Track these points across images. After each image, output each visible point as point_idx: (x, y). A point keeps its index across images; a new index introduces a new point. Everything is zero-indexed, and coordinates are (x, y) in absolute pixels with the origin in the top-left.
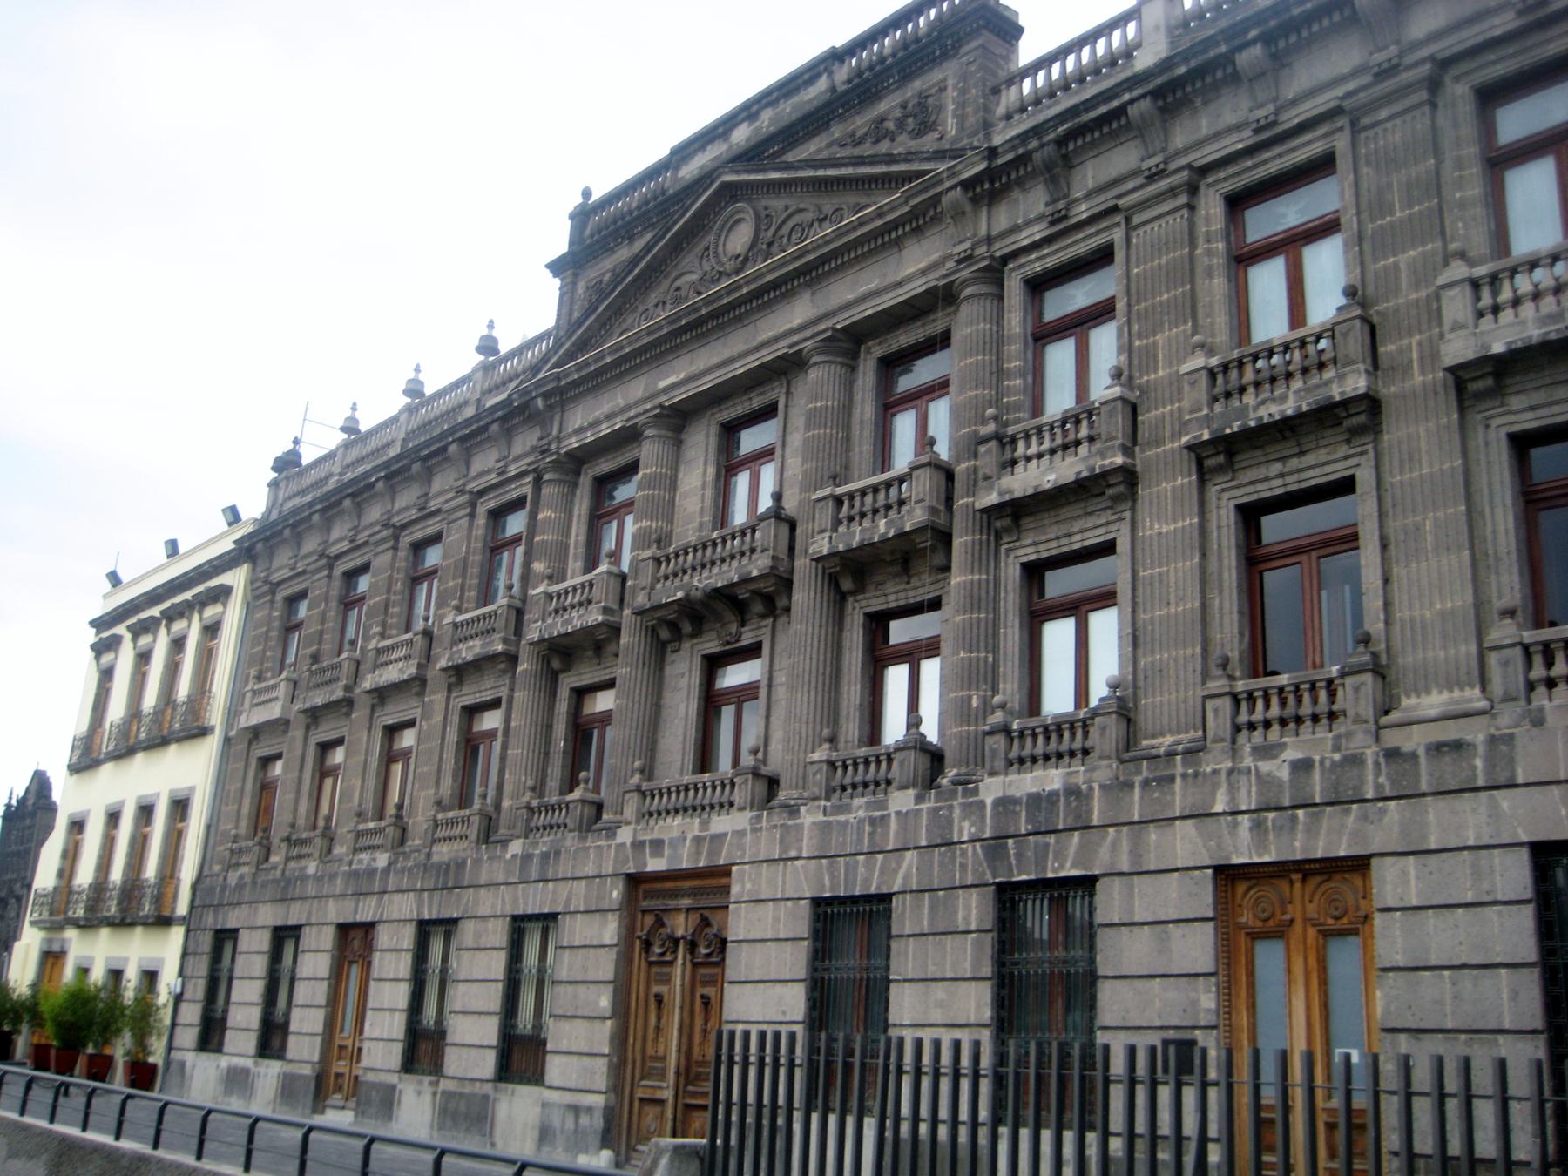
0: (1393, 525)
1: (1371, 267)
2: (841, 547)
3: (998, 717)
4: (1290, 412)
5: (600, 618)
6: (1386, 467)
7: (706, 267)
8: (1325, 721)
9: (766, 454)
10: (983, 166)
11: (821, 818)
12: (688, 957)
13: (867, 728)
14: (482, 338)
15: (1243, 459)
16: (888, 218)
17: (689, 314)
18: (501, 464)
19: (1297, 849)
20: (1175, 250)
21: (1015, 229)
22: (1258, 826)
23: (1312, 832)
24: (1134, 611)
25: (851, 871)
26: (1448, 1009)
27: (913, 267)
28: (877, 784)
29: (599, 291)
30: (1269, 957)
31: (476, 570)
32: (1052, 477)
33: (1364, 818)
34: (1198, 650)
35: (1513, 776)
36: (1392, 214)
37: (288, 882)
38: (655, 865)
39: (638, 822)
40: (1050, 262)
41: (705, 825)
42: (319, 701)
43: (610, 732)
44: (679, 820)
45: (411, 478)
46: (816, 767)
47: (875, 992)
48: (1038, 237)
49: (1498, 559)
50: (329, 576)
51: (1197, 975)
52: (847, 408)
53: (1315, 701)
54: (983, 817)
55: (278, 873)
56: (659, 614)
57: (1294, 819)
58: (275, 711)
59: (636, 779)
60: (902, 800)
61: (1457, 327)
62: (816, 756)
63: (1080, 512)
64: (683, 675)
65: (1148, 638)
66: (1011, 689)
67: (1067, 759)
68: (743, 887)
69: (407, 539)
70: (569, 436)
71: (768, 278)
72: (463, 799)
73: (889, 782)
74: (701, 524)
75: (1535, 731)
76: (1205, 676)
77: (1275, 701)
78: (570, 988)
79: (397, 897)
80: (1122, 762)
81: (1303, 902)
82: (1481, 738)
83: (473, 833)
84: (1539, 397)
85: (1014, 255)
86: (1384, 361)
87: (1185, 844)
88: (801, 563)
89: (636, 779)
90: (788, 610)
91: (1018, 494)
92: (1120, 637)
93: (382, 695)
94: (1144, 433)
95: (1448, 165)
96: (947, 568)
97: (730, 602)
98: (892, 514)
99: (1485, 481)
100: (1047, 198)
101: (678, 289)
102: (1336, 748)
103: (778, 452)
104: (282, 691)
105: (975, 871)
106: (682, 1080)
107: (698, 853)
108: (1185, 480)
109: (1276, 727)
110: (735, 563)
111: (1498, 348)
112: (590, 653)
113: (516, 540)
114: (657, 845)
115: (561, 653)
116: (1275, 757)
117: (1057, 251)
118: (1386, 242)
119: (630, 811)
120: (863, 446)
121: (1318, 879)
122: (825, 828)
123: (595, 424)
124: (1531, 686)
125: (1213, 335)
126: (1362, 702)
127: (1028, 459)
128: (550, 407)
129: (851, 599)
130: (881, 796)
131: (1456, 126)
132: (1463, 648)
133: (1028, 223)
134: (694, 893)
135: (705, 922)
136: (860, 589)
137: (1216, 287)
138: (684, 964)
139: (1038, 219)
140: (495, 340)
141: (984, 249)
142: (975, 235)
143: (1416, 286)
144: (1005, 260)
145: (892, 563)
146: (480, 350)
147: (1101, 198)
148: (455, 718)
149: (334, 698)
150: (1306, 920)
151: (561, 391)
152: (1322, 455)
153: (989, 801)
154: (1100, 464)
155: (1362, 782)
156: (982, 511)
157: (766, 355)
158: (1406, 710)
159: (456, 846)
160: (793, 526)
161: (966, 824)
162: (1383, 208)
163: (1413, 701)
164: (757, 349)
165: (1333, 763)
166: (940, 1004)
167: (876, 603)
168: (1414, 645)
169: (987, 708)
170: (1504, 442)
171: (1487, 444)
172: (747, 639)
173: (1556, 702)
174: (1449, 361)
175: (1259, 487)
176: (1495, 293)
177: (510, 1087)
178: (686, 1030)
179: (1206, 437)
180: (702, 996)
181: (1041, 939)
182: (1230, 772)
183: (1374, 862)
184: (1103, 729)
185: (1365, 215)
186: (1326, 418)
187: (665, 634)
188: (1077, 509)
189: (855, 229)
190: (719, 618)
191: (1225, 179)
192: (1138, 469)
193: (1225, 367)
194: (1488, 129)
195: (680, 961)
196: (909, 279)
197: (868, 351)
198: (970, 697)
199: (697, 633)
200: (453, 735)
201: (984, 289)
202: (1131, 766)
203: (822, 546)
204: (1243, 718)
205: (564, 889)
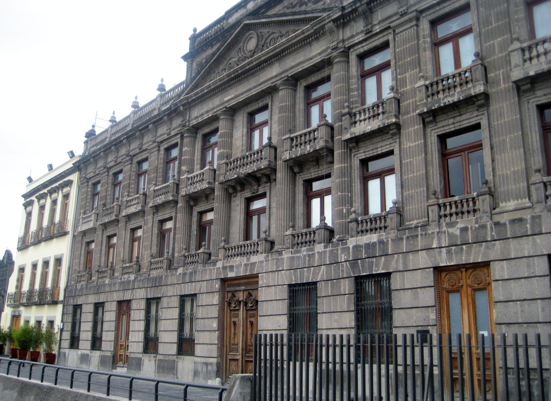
0: (495, 140)
1: (484, 45)
2: (294, 156)
3: (353, 216)
4: (456, 100)
5: (207, 186)
7: (240, 55)
8: (472, 213)
9: (265, 123)
10: (340, 13)
11: (290, 255)
13: (306, 222)
14: (160, 85)
15: (439, 118)
16: (306, 34)
19: (463, 260)
21: (353, 36)
22: (449, 252)
23: (468, 253)
24: (401, 176)
25: (302, 274)
26: (519, 315)
27: (316, 52)
28: (310, 242)
29: (201, 66)
32: (369, 127)
33: (487, 247)
34: (425, 189)
35: (541, 230)
36: (491, 25)
37: (99, 286)
38: (231, 275)
39: (224, 260)
41: (248, 259)
42: (106, 221)
43: (213, 227)
44: (239, 258)
45: (136, 138)
48: (361, 39)
49: (533, 151)
50: (108, 175)
51: (429, 307)
52: (294, 105)
53: (468, 206)
54: (349, 252)
55: (95, 283)
56: (228, 183)
57: (462, 249)
58: (91, 225)
59: (223, 244)
60: (319, 248)
61: (516, 66)
62: (288, 233)
64: (238, 205)
66: (357, 206)
67: (379, 230)
69: (135, 160)
70: (193, 120)
71: (263, 59)
73: (314, 241)
74: (242, 150)
76: (428, 198)
77: (453, 206)
78: (202, 320)
79: (138, 290)
80: (399, 230)
81: (466, 279)
82: (529, 217)
83: (165, 266)
86: (490, 80)
87: (423, 260)
89: (223, 244)
90: (275, 180)
91: (357, 134)
92: (396, 185)
93: (129, 217)
94: (402, 110)
96: (332, 162)
98: (312, 143)
100: (364, 25)
101: (230, 64)
102: (477, 223)
104: (93, 217)
106: (244, 352)
107: (246, 270)
108: (418, 127)
109: (454, 216)
110: (255, 164)
111: (532, 73)
113: (175, 159)
114: (231, 268)
115: (194, 199)
116: (454, 227)
117: (368, 44)
118: (490, 35)
119: (221, 256)
121: (471, 270)
122: (292, 259)
123: (202, 115)
125: (427, 73)
127: (361, 121)
128: (185, 110)
130: (312, 247)
132: (522, 184)
133: (357, 34)
134: (246, 284)
136: (301, 171)
137: (427, 55)
138: (243, 310)
139: (361, 32)
143: (501, 51)
144: (349, 48)
145: (312, 161)
147: (384, 23)
148: (156, 225)
149: (112, 219)
150: (467, 285)
151: (189, 103)
152: (468, 115)
153: (351, 247)
154: (387, 122)
155: (486, 234)
156: (347, 141)
157: (264, 87)
158: (501, 208)
159: (159, 271)
160: (276, 149)
161: (343, 256)
162: (488, 22)
163: (504, 204)
164: (260, 85)
165: (475, 228)
166: (336, 321)
167: (307, 176)
169: (349, 213)
171: (528, 109)
172: (261, 191)
174: (514, 79)
175: (445, 128)
176: (530, 53)
177: (183, 357)
179: (425, 110)
180: (250, 322)
181: (372, 296)
182: (438, 233)
183: (491, 263)
184: (391, 219)
185: (481, 26)
186: (469, 101)
187: (231, 191)
189: (294, 39)
192: (401, 123)
193: (432, 85)
195: (242, 309)
197: (301, 84)
198: (343, 209)
199: (243, 190)
200: (156, 231)
201: (342, 59)
202: (402, 232)
203: (287, 156)
204: (442, 213)
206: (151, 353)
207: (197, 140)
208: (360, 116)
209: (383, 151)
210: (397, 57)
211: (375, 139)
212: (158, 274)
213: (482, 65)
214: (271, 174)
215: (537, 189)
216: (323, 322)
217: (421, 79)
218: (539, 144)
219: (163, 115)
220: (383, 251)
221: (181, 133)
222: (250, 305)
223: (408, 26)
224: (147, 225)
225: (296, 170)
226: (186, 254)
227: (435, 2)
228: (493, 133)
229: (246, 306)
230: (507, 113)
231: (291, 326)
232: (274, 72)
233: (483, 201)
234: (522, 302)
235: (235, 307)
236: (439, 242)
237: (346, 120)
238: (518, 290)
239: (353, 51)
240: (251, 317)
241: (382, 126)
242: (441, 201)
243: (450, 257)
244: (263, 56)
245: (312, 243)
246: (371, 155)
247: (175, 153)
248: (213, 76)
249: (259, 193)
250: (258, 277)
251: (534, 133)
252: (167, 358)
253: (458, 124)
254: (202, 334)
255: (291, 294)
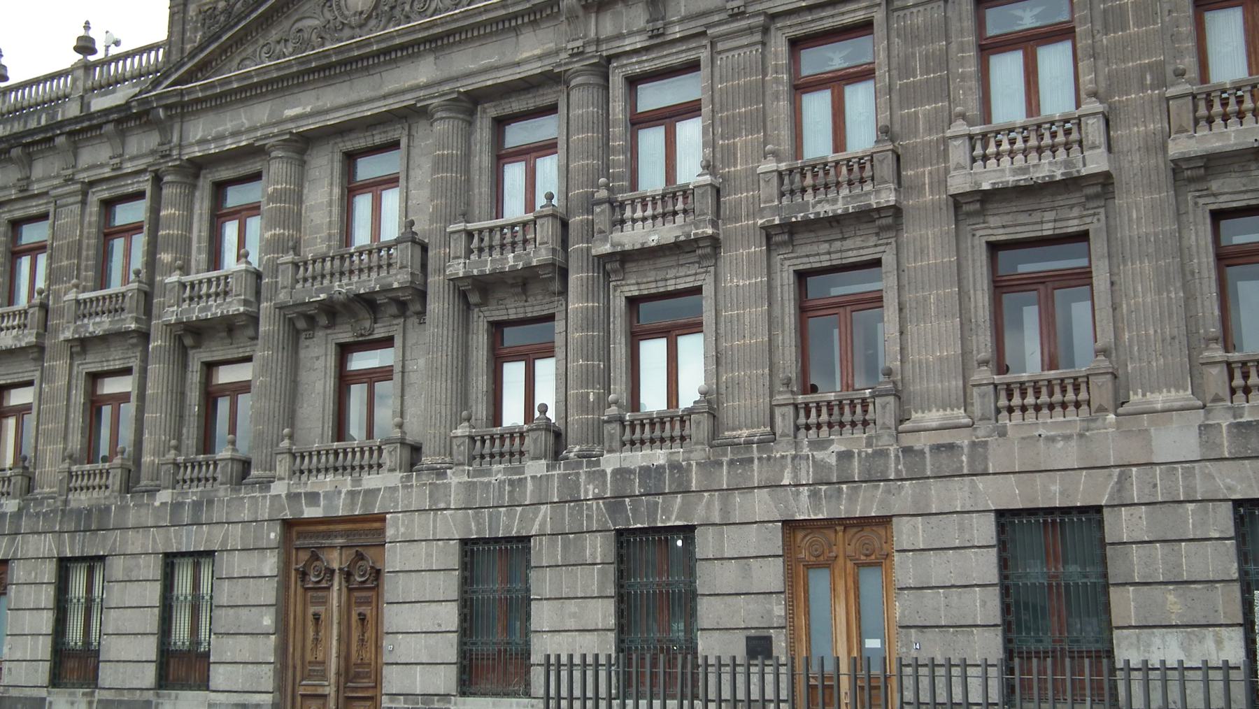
0: (908, 296)
1: (898, 114)
2: (475, 272)
3: (613, 410)
4: (839, 212)
5: (242, 309)
6: (904, 255)
7: (328, 15)
8: (860, 426)
11: (466, 479)
12: (344, 584)
13: (492, 409)
14: (80, 39)
15: (799, 238)
16: (511, 10)
17: (319, 58)
18: (117, 160)
19: (843, 510)
20: (751, 76)
21: (620, 36)
22: (814, 495)
23: (852, 499)
25: (494, 519)
26: (942, 613)
27: (530, 51)
28: (512, 454)
30: (819, 582)
31: (92, 253)
32: (656, 237)
33: (889, 491)
34: (767, 371)
35: (986, 468)
36: (915, 76)
38: (309, 512)
39: (290, 479)
40: (647, 67)
41: (357, 482)
44: (330, 477)
45: (11, 160)
46: (459, 441)
47: (519, 606)
48: (639, 46)
49: (978, 325)
51: (772, 593)
52: (467, 156)
53: (854, 413)
54: (605, 482)
56: (299, 309)
57: (840, 490)
59: (285, 444)
60: (535, 468)
61: (959, 167)
62: (459, 432)
63: (674, 263)
64: (318, 358)
65: (729, 361)
66: (619, 390)
67: (668, 443)
68: (398, 530)
70: (192, 145)
71: (397, 41)
72: (91, 452)
73: (522, 453)
74: (330, 236)
75: (1001, 440)
77: (824, 410)
78: (231, 611)
79: (32, 539)
80: (711, 447)
81: (844, 545)
82: (966, 442)
83: (115, 480)
84: (1007, 219)
85: (617, 56)
86: (905, 182)
87: (761, 505)
88: (434, 280)
89: (285, 444)
90: (422, 313)
91: (627, 248)
92: (705, 357)
94: (725, 211)
95: (954, 46)
96: (564, 292)
97: (368, 303)
99: (971, 273)
100: (647, 17)
101: (300, 31)
102: (869, 445)
103: (402, 182)
105: (598, 521)
106: (342, 680)
107: (353, 504)
108: (758, 249)
109: (825, 428)
110: (374, 275)
111: (986, 186)
112: (224, 334)
113: (132, 229)
114: (313, 498)
115: (192, 334)
116: (826, 449)
117: (653, 59)
118: (910, 96)
120: (482, 190)
121: (855, 530)
122: (470, 487)
123: (220, 138)
124: (998, 411)
125: (779, 144)
126: (887, 415)
127: (634, 221)
128: (170, 117)
129: (476, 310)
130: (517, 464)
131: (960, 20)
132: (954, 383)
133: (631, 34)
134: (347, 534)
135: (360, 557)
136: (484, 303)
138: (340, 590)
139: (639, 32)
140: (92, 41)
141: (593, 48)
142: (585, 36)
143: (930, 131)
144: (609, 59)
145: (513, 285)
146: (78, 49)
147: (693, 24)
148: (81, 383)
150: (846, 557)
151: (183, 105)
152: (858, 242)
153: (609, 471)
154: (694, 232)
155: (887, 468)
156: (600, 257)
158: (914, 422)
160: (424, 249)
161: (591, 487)
162: (907, 71)
163: (919, 415)
164: (385, 97)
165: (867, 454)
166: (574, 615)
168: (921, 378)
169: (602, 403)
170: (984, 245)
171: (973, 247)
172: (380, 333)
173: (1014, 422)
174: (952, 191)
175: (812, 259)
176: (985, 147)
177: (173, 693)
178: (344, 640)
179: (777, 222)
180: (360, 614)
181: (652, 570)
182: (794, 458)
183: (894, 519)
184: (698, 423)
185: (894, 73)
186: (865, 216)
187: (301, 324)
188: (671, 261)
189: (480, 14)
190: (354, 315)
191: (790, 26)
192: (721, 237)
194: (980, 24)
195: (336, 587)
196: (527, 61)
197: (484, 111)
198: (588, 394)
200: (78, 397)
201: (592, 80)
202: (719, 449)
203: (458, 269)
204: (802, 420)
205: (219, 532)
206: (73, 686)
207: (197, 194)
208: (634, 211)
209: (679, 287)
210: (717, 99)
211: (662, 260)
212: (93, 502)
213: (893, 151)
214: (411, 300)
215: (983, 396)
216: (542, 615)
217: (770, 158)
218: (987, 313)
219: (103, 119)
220: (680, 485)
221: (156, 172)
222: (314, 579)
223: (745, 41)
224: (50, 381)
225: (474, 298)
226: (181, 459)
227: (804, 4)
228: (905, 281)
229: (348, 580)
230: (934, 249)
231: (467, 625)
232: (421, 73)
233: (884, 407)
234: (947, 590)
235: (318, 582)
236: (796, 476)
237: (602, 215)
238: (941, 569)
239: (617, 67)
240: (359, 604)
241: (682, 238)
242: (800, 399)
243: (816, 507)
244: (399, 36)
245: (517, 456)
246: (653, 291)
247: (126, 215)
248: (250, 50)
249: (376, 336)
250: (384, 520)
251: (979, 293)
252: (126, 697)
253: (839, 255)
254: (230, 641)
255: (468, 559)
